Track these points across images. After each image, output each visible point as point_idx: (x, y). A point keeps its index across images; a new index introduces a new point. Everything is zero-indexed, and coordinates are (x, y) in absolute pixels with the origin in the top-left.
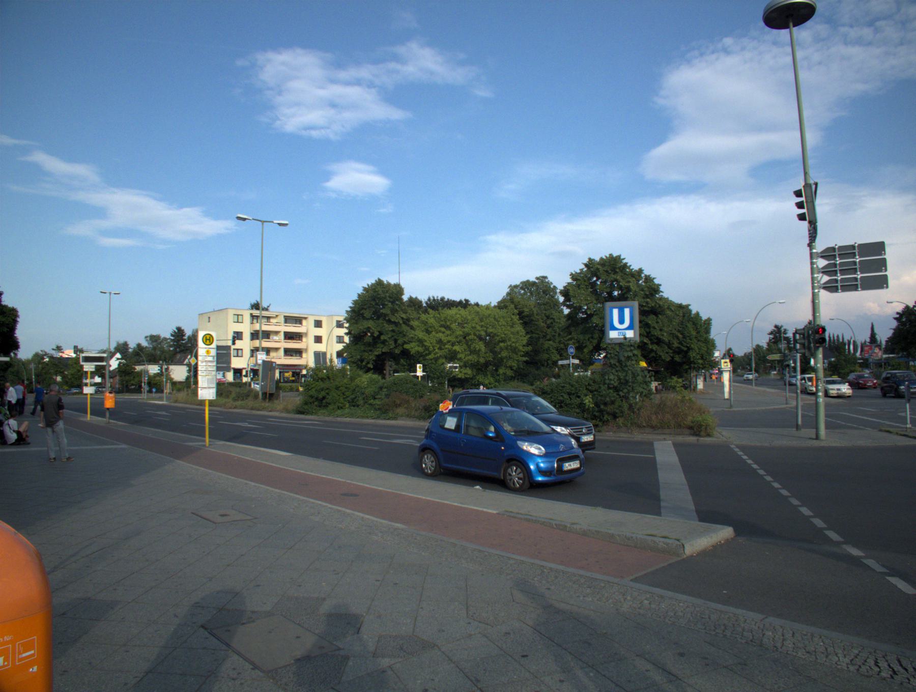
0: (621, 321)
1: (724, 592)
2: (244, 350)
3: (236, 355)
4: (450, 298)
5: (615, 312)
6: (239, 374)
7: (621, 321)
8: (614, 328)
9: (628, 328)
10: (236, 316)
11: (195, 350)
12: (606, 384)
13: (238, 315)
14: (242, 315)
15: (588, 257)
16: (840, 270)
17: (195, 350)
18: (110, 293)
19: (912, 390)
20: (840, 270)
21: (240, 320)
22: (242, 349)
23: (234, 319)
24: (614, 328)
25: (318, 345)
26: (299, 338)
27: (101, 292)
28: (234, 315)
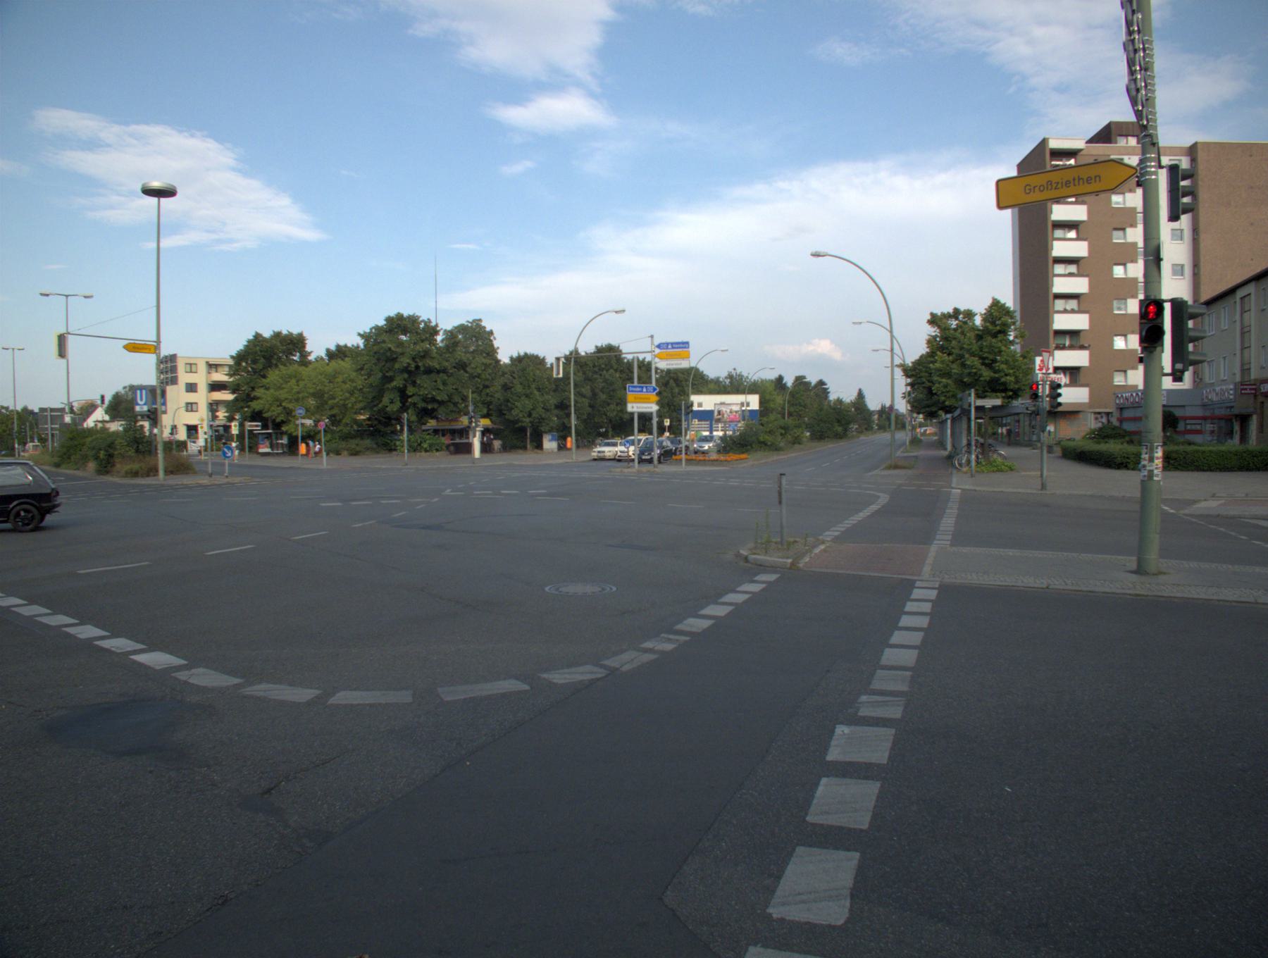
0: (141, 400)
1: (113, 946)
2: (199, 404)
3: (189, 370)
4: (913, 360)
5: (260, 424)
6: (194, 432)
7: (141, 400)
8: (138, 404)
9: (145, 404)
10: (188, 366)
11: (1184, 517)
12: (281, 406)
13: (191, 364)
14: (196, 364)
15: (929, 312)
16: (52, 424)
17: (1184, 517)
18: (13, 349)
19: (139, 392)
20: (52, 424)
21: (194, 370)
22: (196, 403)
23: (197, 367)
24: (138, 404)
25: (701, 401)
26: (646, 420)
27: (3, 348)
28: (186, 364)
